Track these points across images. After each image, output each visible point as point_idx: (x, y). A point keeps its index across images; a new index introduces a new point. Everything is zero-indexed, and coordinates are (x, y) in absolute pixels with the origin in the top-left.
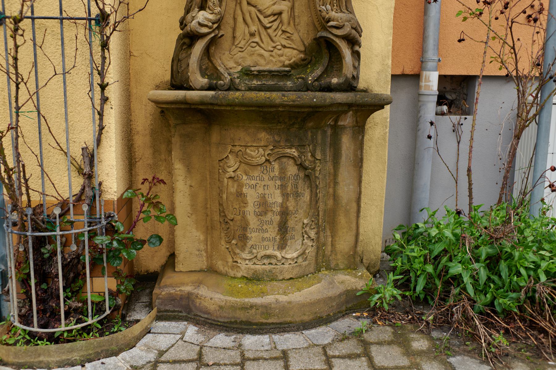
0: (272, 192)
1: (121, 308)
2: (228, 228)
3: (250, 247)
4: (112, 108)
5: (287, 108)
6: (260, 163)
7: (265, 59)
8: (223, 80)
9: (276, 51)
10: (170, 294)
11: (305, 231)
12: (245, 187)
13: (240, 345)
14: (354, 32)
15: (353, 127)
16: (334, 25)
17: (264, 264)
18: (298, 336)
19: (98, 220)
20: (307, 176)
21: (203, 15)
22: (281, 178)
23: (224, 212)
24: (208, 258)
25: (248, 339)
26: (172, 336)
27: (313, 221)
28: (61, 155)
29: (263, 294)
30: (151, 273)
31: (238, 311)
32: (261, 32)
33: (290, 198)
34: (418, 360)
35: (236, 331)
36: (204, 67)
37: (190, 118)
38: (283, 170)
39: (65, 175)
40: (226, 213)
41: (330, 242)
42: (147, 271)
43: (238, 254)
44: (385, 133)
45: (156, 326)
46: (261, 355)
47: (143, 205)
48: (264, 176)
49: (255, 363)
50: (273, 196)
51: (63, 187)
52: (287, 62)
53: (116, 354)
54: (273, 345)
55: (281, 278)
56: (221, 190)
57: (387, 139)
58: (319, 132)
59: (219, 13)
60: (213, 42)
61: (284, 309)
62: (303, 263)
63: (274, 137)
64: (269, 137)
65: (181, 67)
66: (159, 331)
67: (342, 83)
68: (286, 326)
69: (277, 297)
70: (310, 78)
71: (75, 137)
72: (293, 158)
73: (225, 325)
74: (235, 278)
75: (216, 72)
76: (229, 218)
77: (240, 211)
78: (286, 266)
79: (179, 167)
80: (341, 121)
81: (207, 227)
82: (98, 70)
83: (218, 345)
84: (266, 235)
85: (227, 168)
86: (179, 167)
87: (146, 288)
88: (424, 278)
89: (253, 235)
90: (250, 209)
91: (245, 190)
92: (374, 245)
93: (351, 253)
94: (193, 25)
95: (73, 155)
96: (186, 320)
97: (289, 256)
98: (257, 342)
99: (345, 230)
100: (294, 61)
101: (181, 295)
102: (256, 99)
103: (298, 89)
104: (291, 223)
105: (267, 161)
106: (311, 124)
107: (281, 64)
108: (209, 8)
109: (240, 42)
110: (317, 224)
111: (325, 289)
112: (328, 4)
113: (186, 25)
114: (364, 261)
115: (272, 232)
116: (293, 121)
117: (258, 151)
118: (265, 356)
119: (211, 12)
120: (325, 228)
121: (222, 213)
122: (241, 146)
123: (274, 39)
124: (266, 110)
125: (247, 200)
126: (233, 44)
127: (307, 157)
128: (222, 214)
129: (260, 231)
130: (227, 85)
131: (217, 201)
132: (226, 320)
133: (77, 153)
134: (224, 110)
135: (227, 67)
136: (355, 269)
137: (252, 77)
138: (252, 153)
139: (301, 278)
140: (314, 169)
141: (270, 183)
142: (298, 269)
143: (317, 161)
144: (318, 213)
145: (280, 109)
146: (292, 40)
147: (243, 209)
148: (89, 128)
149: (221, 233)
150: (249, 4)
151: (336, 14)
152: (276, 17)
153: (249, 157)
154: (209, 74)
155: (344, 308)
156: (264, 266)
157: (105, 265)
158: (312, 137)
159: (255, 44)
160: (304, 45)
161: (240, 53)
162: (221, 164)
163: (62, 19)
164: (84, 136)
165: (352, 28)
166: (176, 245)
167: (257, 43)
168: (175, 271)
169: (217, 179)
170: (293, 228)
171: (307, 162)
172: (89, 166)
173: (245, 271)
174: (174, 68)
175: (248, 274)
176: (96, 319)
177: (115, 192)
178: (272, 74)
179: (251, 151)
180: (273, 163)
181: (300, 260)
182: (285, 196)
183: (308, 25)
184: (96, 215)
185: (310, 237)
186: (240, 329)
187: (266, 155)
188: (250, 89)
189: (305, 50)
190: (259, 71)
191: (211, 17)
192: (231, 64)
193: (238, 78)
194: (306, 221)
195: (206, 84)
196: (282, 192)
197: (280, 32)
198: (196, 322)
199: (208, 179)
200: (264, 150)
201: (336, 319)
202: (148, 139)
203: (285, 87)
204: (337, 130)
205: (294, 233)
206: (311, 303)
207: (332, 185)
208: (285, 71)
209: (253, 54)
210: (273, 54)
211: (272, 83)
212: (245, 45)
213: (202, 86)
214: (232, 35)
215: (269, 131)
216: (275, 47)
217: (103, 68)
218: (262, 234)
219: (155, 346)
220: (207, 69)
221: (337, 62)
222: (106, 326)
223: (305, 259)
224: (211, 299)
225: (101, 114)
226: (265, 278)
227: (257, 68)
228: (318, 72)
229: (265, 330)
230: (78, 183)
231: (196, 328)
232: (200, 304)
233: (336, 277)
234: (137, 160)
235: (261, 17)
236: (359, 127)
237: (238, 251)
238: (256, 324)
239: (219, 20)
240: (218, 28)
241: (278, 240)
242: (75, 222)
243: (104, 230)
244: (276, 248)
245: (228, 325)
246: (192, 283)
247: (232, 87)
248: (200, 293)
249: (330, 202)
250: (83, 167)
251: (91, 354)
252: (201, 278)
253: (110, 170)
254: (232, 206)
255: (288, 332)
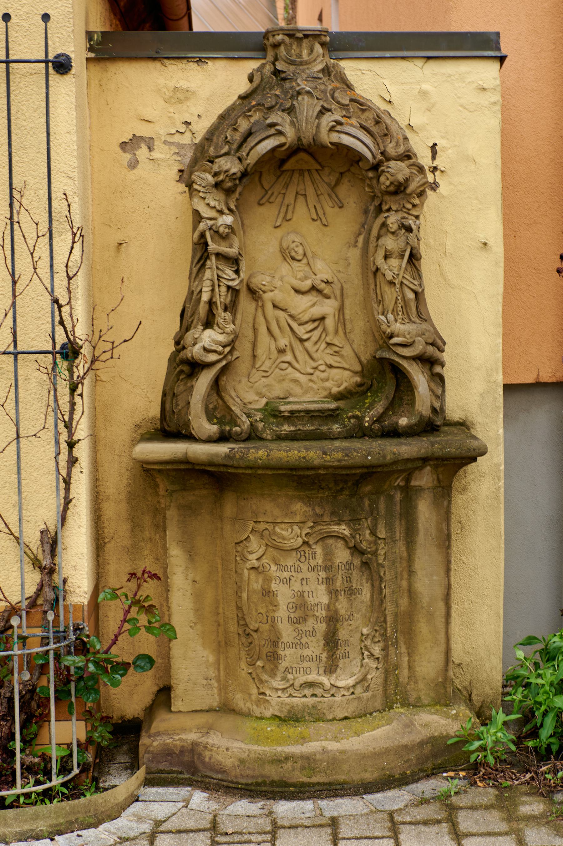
0: (313, 588)
1: (92, 769)
2: (251, 643)
3: (283, 670)
4: (81, 472)
5: (331, 471)
6: (295, 547)
7: (302, 387)
8: (239, 426)
9: (317, 373)
10: (165, 744)
11: (365, 646)
12: (274, 582)
13: (271, 813)
14: (431, 349)
15: (434, 488)
16: (399, 342)
17: (305, 696)
18: (355, 801)
19: (62, 634)
20: (366, 564)
21: (210, 337)
22: (327, 568)
23: (244, 620)
24: (220, 690)
25: (282, 805)
26: (172, 804)
27: (376, 631)
28: (8, 541)
29: (303, 739)
30: (129, 721)
31: (267, 766)
32: (295, 346)
33: (340, 597)
34: (521, 826)
35: (265, 796)
36: (211, 406)
37: (192, 481)
38: (328, 555)
39: (14, 569)
40: (247, 620)
41: (406, 663)
42: (122, 717)
43: (266, 681)
44: (498, 489)
45: (145, 794)
46: (299, 822)
47: (127, 612)
48: (301, 565)
49: (292, 831)
50: (314, 595)
51: (11, 587)
52: (335, 390)
53: (95, 825)
54: (318, 812)
55: (330, 717)
56: (240, 587)
57: (502, 498)
58: (382, 498)
59: (233, 332)
60: (224, 370)
61: (335, 761)
62: (365, 694)
63: (314, 510)
64: (307, 509)
65: (177, 405)
66: (151, 798)
67: (415, 425)
68: (338, 787)
69: (325, 743)
70: (367, 419)
71: (29, 514)
72: (343, 538)
73: (249, 788)
74: (261, 718)
75: (229, 413)
76: (252, 627)
77: (267, 616)
78: (338, 698)
79: (176, 554)
80: (416, 480)
81: (219, 642)
82: (65, 421)
83: (238, 813)
84: (306, 652)
85: (248, 555)
86: (176, 554)
87: (123, 744)
88: (553, 718)
89: (288, 652)
90: (282, 613)
91: (274, 586)
92: (489, 670)
93: (440, 680)
94: (196, 352)
95: (26, 540)
96: (190, 785)
97: (341, 684)
98: (296, 809)
99: (428, 645)
100: (346, 388)
101: (183, 747)
102: (286, 459)
103: (349, 436)
104: (343, 634)
105: (305, 543)
106: (368, 488)
107: (325, 393)
108: (218, 324)
109: (263, 363)
110: (384, 635)
111: (398, 733)
112: (390, 312)
113: (184, 348)
114: (474, 697)
115: (315, 648)
116: (341, 486)
117: (292, 529)
118: (306, 824)
119: (220, 331)
120: (397, 642)
121: (242, 621)
122: (268, 522)
123: (315, 356)
124: (301, 473)
125: (277, 601)
126: (253, 366)
127: (364, 535)
128: (242, 622)
129: (298, 647)
130: (246, 433)
131: (234, 604)
132: (250, 781)
133: (32, 537)
134: (243, 474)
135: (245, 401)
136: (447, 705)
137: (282, 420)
138: (283, 532)
139: (361, 717)
140: (375, 553)
141: (312, 576)
142: (356, 703)
143: (380, 542)
144: (385, 618)
145: (321, 472)
146: (342, 356)
147: (272, 615)
148: (49, 501)
149: (240, 650)
150: (275, 306)
151: (402, 327)
152: (316, 324)
153: (279, 538)
154: (218, 416)
155: (429, 765)
156: (304, 699)
157: (73, 699)
158: (370, 506)
159: (287, 365)
160: (360, 362)
161: (263, 379)
162: (239, 549)
163: (16, 355)
164: (42, 512)
165: (426, 343)
166: (172, 670)
167: (289, 363)
168: (171, 712)
169: (234, 570)
170: (347, 642)
171: (364, 543)
172: (49, 556)
173: (277, 707)
174: (168, 406)
175: (281, 711)
176: (61, 779)
177: (85, 593)
178: (311, 415)
179: (282, 529)
180: (314, 547)
181: (359, 690)
182: (333, 593)
183: (365, 332)
184: (59, 627)
185: (372, 655)
186: (271, 792)
187: (303, 535)
188: (279, 438)
189: (362, 371)
190: (292, 412)
191: (221, 338)
192: (250, 396)
193: (261, 420)
194: (365, 631)
195: (215, 434)
196: (329, 587)
197: (324, 345)
198: (205, 788)
199: (220, 569)
200: (300, 528)
201: (417, 781)
202: (123, 507)
203: (330, 433)
204: (409, 494)
205: (348, 648)
206: (375, 754)
207: (406, 576)
208: (329, 410)
209: (283, 380)
210: (314, 378)
211: (312, 428)
212: (270, 368)
213: (210, 436)
214: (251, 353)
215: (308, 501)
216: (316, 368)
217: (71, 418)
218: (300, 651)
219: (149, 816)
220: (215, 408)
221: (407, 391)
222: (73, 790)
223: (367, 689)
224: (227, 749)
225: (67, 482)
226: (307, 718)
227: (289, 407)
228: (379, 408)
229: (308, 794)
230: (33, 579)
231: (206, 795)
232: (210, 758)
233: (416, 717)
234: (106, 540)
235: (294, 325)
236: (443, 488)
237: (265, 677)
238: (294, 785)
239: (233, 341)
240: (231, 352)
241: (324, 659)
242: (28, 638)
243: (72, 648)
244: (321, 671)
245: (253, 788)
246: (198, 729)
247: (253, 434)
248: (210, 741)
249: (404, 602)
250: (40, 557)
251: (61, 824)
252: (211, 721)
253: (78, 560)
254: (256, 610)
255: (342, 796)
